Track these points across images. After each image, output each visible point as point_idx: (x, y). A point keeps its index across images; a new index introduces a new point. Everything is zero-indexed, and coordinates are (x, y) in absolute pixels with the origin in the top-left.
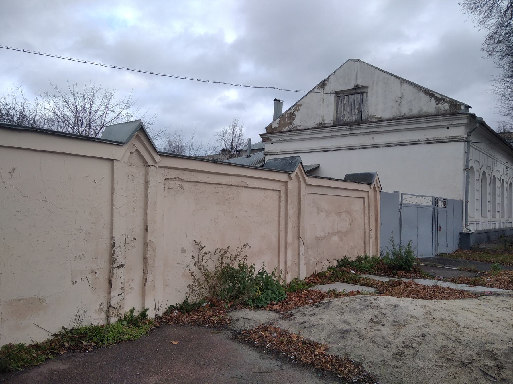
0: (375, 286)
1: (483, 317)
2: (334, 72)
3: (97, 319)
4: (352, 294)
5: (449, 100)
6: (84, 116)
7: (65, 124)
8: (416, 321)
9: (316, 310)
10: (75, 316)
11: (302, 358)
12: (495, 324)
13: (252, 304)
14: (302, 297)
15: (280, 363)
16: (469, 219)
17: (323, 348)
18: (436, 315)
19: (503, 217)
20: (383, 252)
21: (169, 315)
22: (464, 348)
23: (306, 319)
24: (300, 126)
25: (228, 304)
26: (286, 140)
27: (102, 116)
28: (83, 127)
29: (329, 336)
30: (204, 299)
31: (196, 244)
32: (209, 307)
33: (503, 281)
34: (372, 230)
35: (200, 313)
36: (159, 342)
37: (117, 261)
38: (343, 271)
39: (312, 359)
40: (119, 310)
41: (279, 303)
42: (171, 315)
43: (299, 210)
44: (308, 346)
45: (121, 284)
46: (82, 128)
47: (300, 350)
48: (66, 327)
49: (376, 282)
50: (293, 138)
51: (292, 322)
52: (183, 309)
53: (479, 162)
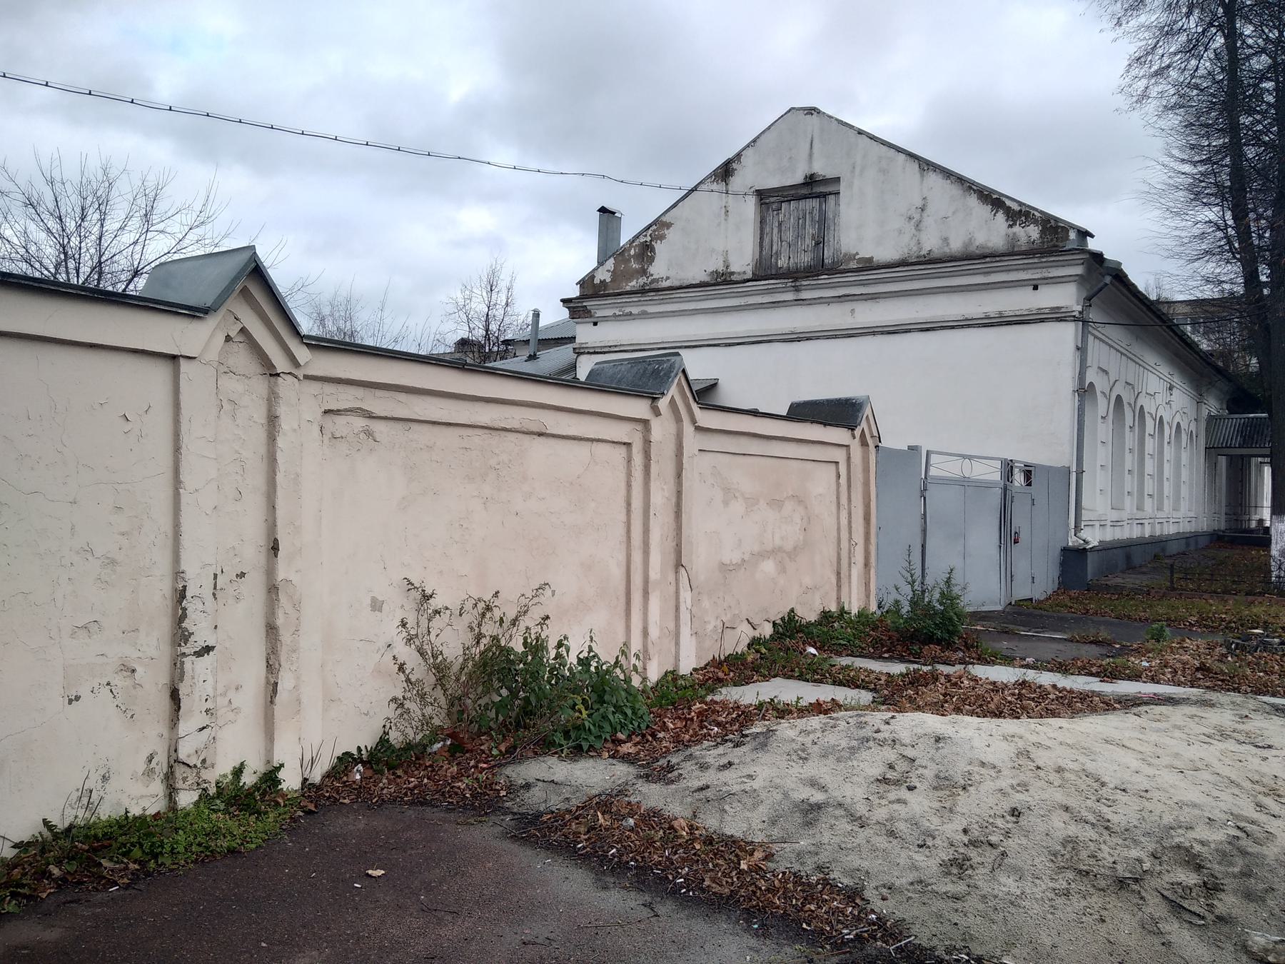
0: (873, 686)
1: (1156, 761)
2: (754, 141)
3: (142, 797)
4: (818, 708)
5: (1039, 215)
6: (83, 244)
7: (32, 266)
8: (994, 775)
9: (735, 754)
10: (78, 790)
11: (707, 883)
12: (1190, 778)
13: (563, 742)
14: (692, 719)
15: (648, 898)
16: (1086, 515)
17: (758, 855)
18: (1042, 758)
19: (1160, 509)
20: (885, 599)
21: (341, 778)
22: (1120, 842)
23: (710, 777)
24: (668, 278)
25: (499, 744)
26: (631, 314)
27: (132, 246)
28: (81, 275)
29: (773, 823)
30: (436, 734)
31: (410, 587)
32: (446, 754)
33: (1178, 665)
34: (856, 544)
35: (423, 770)
36: (316, 855)
37: (192, 639)
38: (789, 649)
39: (732, 883)
40: (203, 771)
41: (633, 737)
42: (345, 779)
43: (679, 493)
44: (721, 848)
45: (206, 700)
46: (78, 277)
47: (698, 860)
48: (55, 820)
49: (872, 676)
50: (651, 309)
51: (674, 786)
52: (378, 762)
53: (1106, 372)
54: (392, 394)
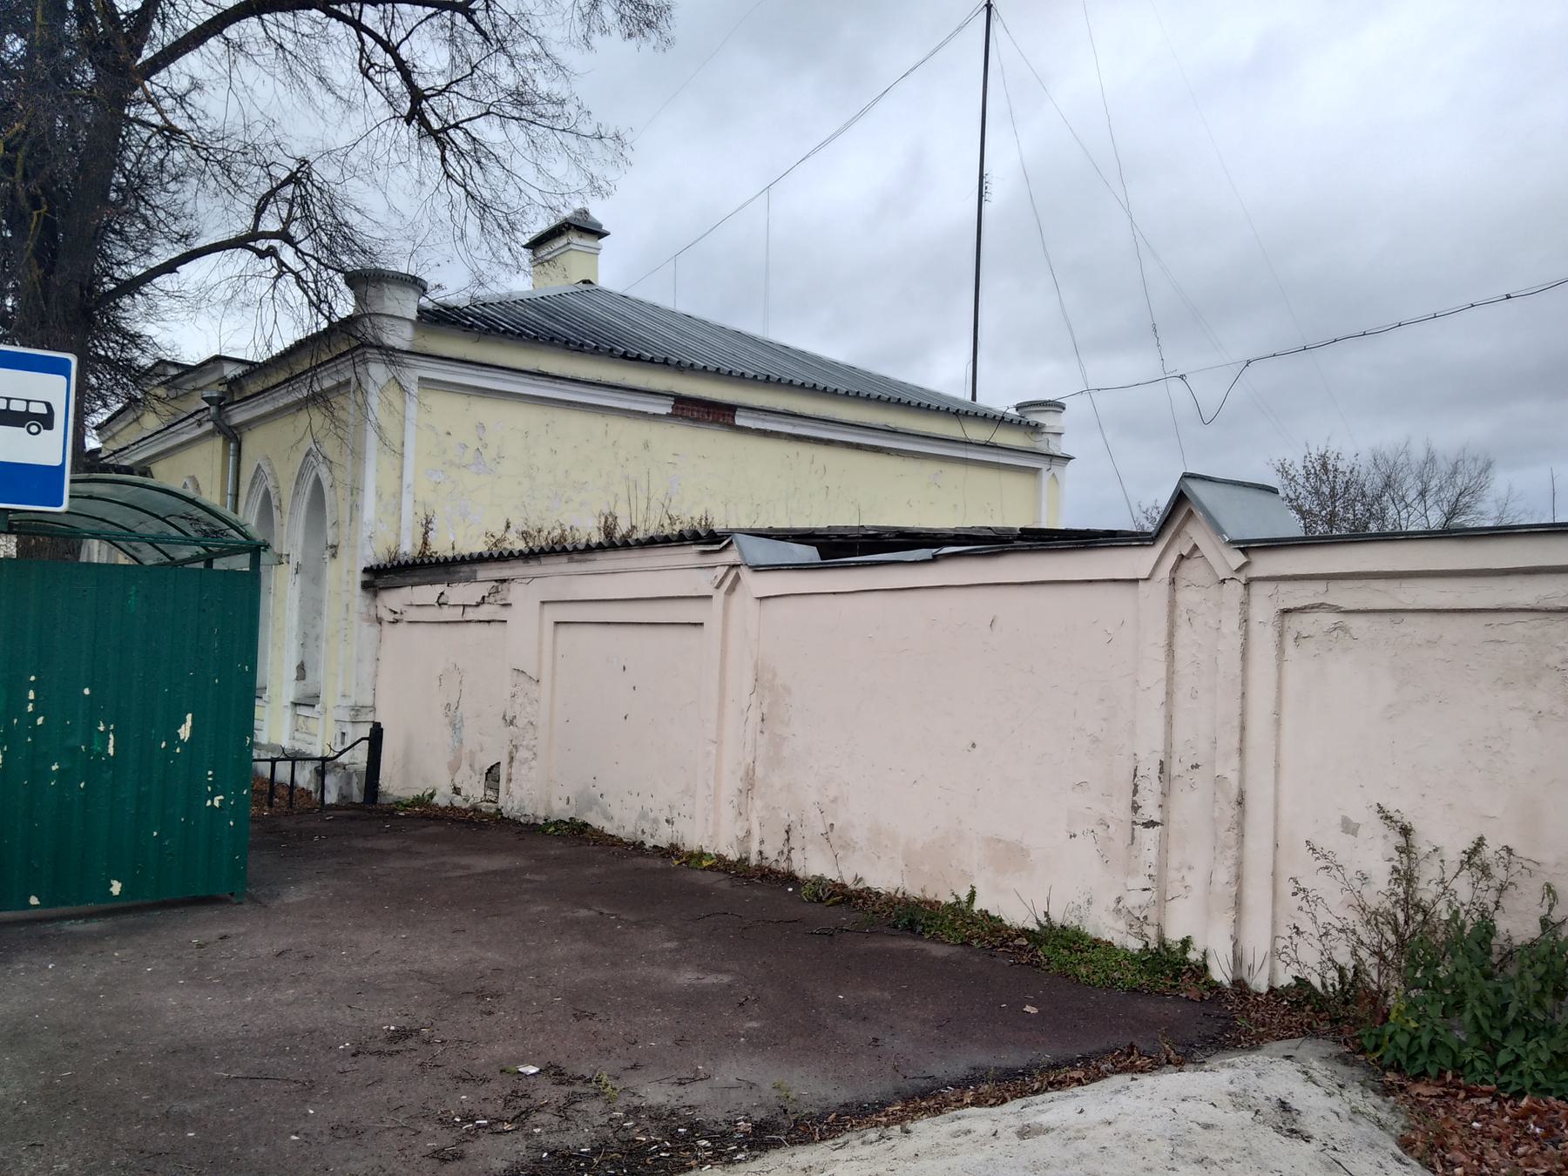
54: (1364, 582)
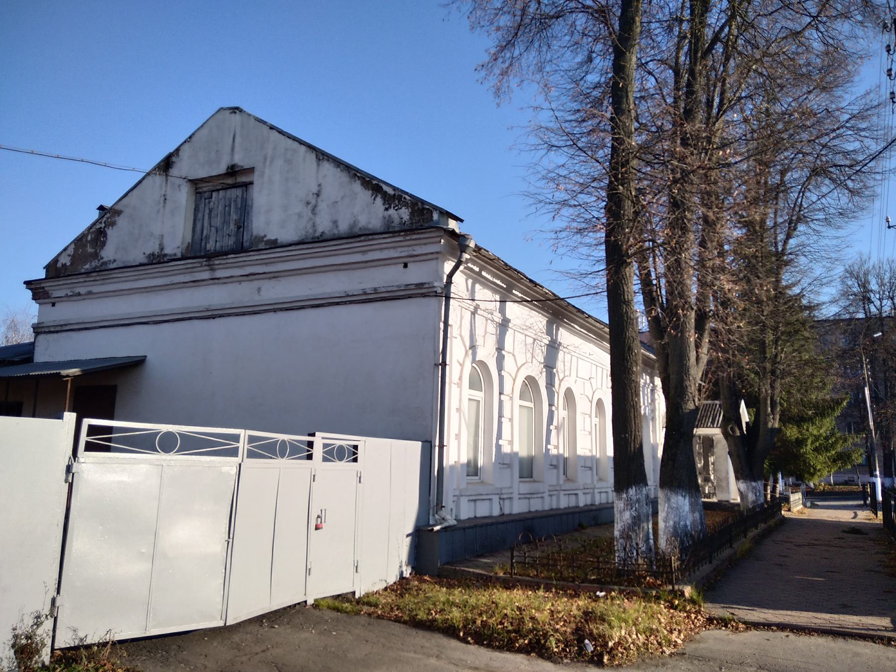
2: (190, 137)
5: (409, 198)
24: (115, 261)
26: (79, 294)
50: (95, 289)
